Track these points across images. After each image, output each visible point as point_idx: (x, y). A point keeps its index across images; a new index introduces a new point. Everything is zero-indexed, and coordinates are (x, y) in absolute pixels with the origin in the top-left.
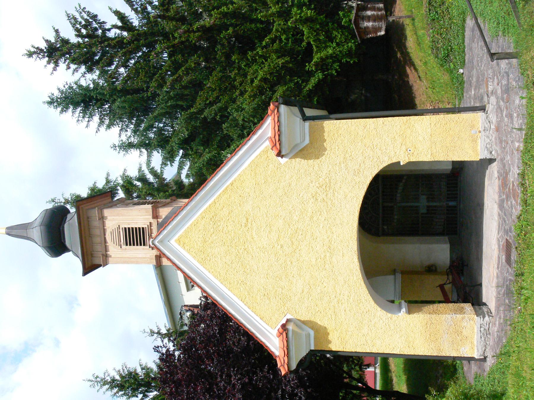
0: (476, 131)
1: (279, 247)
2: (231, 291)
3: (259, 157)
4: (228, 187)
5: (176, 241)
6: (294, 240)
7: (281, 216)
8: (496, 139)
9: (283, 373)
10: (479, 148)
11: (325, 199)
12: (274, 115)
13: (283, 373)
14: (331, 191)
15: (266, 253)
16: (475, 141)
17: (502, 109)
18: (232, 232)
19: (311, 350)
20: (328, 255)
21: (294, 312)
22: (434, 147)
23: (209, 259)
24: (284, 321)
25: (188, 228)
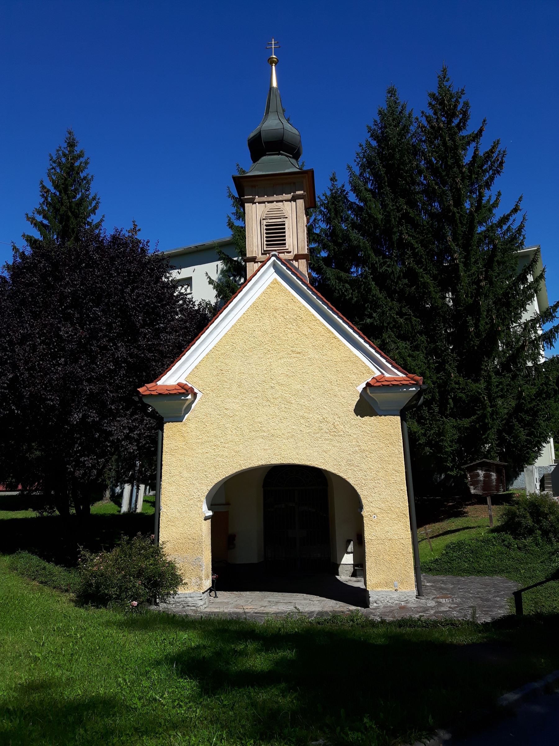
0: (397, 586)
1: (273, 385)
2: (224, 336)
3: (363, 365)
4: (333, 334)
5: (276, 279)
6: (280, 399)
7: (303, 387)
8: (391, 607)
9: (141, 390)
10: (379, 589)
11: (322, 431)
12: (409, 381)
13: (141, 390)
14: (331, 437)
15: (266, 372)
16: (387, 584)
17: (426, 612)
18: (286, 338)
19: (163, 418)
20: (265, 434)
21: (204, 401)
22: (379, 542)
23: (258, 313)
24: (196, 391)
25: (289, 292)
